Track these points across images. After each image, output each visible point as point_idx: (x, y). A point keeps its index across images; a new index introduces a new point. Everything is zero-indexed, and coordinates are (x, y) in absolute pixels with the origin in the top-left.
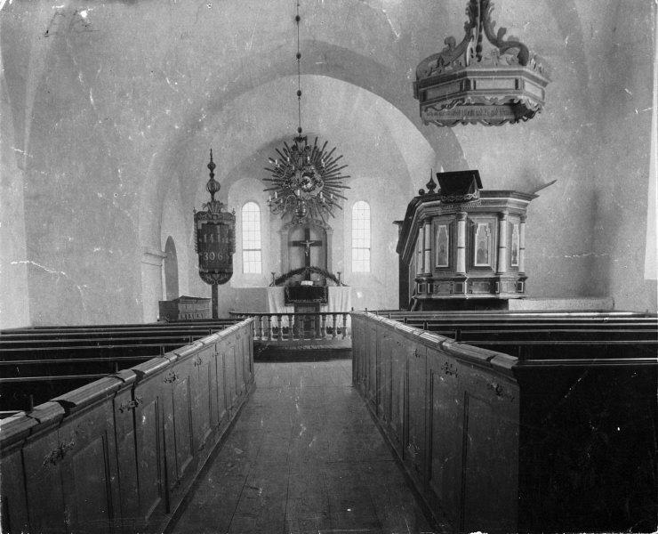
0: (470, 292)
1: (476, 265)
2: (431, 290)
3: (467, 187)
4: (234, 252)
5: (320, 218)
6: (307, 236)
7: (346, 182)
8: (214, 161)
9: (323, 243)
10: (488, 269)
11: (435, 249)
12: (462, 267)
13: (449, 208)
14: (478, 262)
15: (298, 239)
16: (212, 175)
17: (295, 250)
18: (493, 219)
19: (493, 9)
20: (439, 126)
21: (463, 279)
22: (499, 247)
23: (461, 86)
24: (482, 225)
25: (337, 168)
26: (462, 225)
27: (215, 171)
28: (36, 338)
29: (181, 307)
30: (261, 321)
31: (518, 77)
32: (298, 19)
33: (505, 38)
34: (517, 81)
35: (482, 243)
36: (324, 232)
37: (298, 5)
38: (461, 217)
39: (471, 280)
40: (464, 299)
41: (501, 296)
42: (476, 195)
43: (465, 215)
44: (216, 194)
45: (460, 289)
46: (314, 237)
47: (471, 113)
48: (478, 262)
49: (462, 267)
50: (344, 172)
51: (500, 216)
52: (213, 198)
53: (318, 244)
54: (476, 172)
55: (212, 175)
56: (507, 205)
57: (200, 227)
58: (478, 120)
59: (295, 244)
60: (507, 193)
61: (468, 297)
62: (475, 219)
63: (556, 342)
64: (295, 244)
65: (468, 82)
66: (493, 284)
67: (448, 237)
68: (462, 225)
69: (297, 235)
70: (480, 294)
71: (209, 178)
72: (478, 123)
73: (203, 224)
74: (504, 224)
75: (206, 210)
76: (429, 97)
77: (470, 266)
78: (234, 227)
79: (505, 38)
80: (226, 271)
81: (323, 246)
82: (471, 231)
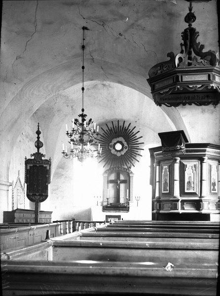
0: (183, 208)
1: (186, 191)
2: (160, 207)
3: (177, 141)
4: (49, 183)
5: (126, 167)
6: (118, 177)
7: (141, 146)
8: (40, 130)
9: (128, 181)
10: (194, 194)
11: (162, 181)
12: (177, 192)
13: (169, 155)
14: (187, 189)
15: (113, 179)
16: (38, 138)
17: (111, 185)
18: (196, 162)
19: (199, 35)
20: (168, 106)
21: (178, 201)
22: (201, 180)
23: (174, 80)
24: (190, 164)
25: (136, 138)
26: (177, 167)
27: (40, 136)
28: (158, 224)
29: (16, 215)
30: (84, 225)
31: (210, 73)
32: (83, 47)
33: (204, 51)
34: (209, 76)
35: (190, 177)
36: (128, 175)
37: (84, 39)
38: (176, 161)
39: (183, 202)
40: (178, 213)
41: (204, 211)
42: (183, 146)
43: (178, 159)
44: (40, 149)
45: (176, 208)
46: (122, 177)
47: (189, 98)
48: (187, 189)
49: (177, 192)
50: (140, 141)
51: (201, 160)
52: (38, 151)
53: (124, 182)
54: (182, 132)
55: (38, 138)
56: (206, 153)
57: (29, 168)
58: (192, 102)
59: (111, 182)
60: (205, 145)
61: (180, 211)
62: (185, 162)
63: (23, 266)
64: (111, 182)
65: (178, 77)
66: (197, 204)
67: (168, 173)
68: (177, 167)
69: (113, 177)
70: (189, 209)
71: (37, 139)
72: (193, 104)
73: (30, 167)
74: (205, 166)
75: (33, 158)
76: (156, 88)
77: (182, 192)
78: (50, 168)
79: (204, 51)
80: (44, 194)
81: (128, 183)
82: (183, 168)
